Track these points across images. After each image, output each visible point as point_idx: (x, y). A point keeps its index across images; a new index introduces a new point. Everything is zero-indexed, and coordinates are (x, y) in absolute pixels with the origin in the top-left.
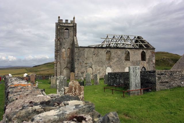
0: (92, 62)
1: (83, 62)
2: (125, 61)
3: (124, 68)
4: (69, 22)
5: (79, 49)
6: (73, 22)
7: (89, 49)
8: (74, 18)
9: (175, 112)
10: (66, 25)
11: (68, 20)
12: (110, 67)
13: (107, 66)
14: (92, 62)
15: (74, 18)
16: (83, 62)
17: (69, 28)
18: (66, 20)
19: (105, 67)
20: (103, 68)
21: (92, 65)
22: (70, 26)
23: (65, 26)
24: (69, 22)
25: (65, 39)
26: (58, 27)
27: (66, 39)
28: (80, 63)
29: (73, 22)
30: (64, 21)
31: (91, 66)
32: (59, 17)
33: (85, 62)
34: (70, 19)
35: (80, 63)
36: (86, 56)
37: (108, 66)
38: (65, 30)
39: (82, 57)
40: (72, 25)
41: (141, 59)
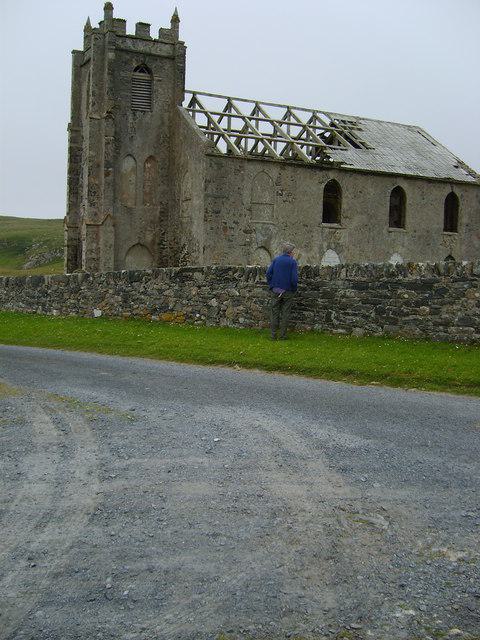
0: (271, 227)
1: (237, 223)
2: (391, 229)
3: (389, 255)
4: (154, 35)
5: (220, 166)
6: (170, 36)
7: (259, 167)
8: (175, 20)
9: (246, 474)
10: (141, 47)
11: (125, 21)
12: (335, 249)
13: (325, 244)
14: (271, 227)
15: (175, 20)
16: (237, 223)
17: (153, 66)
18: (141, 24)
19: (316, 249)
20: (309, 255)
21: (270, 238)
22: (159, 56)
23: (138, 53)
24: (154, 35)
25: (134, 112)
26: (103, 53)
27: (138, 113)
28: (225, 229)
29: (170, 36)
30: (131, 30)
31: (266, 242)
32: (109, 8)
33: (243, 224)
34: (158, 24)
35: (225, 229)
36: (247, 200)
37: (329, 248)
38: (135, 70)
39: (232, 199)
40: (165, 50)
41: (442, 226)
